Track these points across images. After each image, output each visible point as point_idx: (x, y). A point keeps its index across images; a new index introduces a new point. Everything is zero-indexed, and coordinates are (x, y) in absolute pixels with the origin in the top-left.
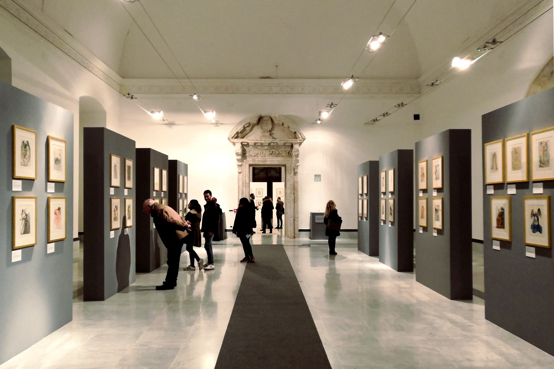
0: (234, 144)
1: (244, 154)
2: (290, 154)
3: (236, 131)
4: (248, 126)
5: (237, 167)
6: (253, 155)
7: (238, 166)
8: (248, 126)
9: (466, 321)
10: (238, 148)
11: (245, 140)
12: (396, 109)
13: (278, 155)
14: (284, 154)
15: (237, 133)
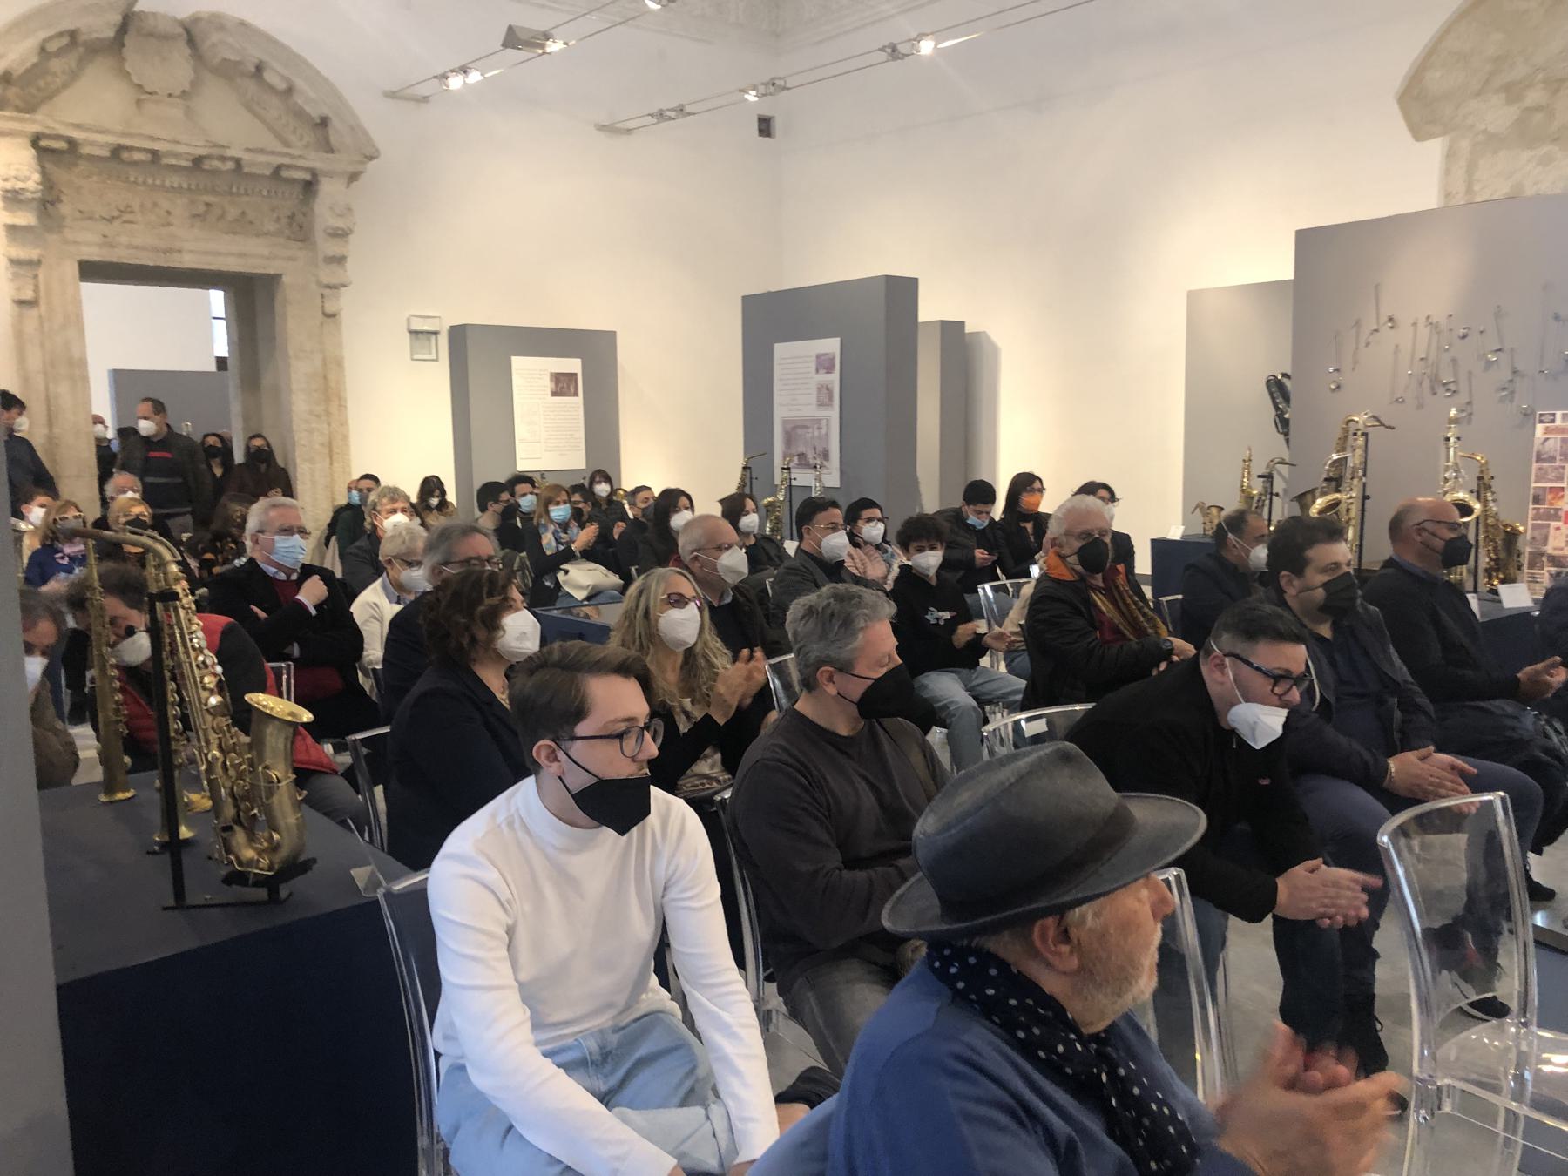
1: (47, 202)
2: (299, 230)
4: (60, 53)
7: (15, 262)
8: (60, 53)
11: (38, 122)
12: (651, 120)
13: (241, 226)
14: (271, 226)
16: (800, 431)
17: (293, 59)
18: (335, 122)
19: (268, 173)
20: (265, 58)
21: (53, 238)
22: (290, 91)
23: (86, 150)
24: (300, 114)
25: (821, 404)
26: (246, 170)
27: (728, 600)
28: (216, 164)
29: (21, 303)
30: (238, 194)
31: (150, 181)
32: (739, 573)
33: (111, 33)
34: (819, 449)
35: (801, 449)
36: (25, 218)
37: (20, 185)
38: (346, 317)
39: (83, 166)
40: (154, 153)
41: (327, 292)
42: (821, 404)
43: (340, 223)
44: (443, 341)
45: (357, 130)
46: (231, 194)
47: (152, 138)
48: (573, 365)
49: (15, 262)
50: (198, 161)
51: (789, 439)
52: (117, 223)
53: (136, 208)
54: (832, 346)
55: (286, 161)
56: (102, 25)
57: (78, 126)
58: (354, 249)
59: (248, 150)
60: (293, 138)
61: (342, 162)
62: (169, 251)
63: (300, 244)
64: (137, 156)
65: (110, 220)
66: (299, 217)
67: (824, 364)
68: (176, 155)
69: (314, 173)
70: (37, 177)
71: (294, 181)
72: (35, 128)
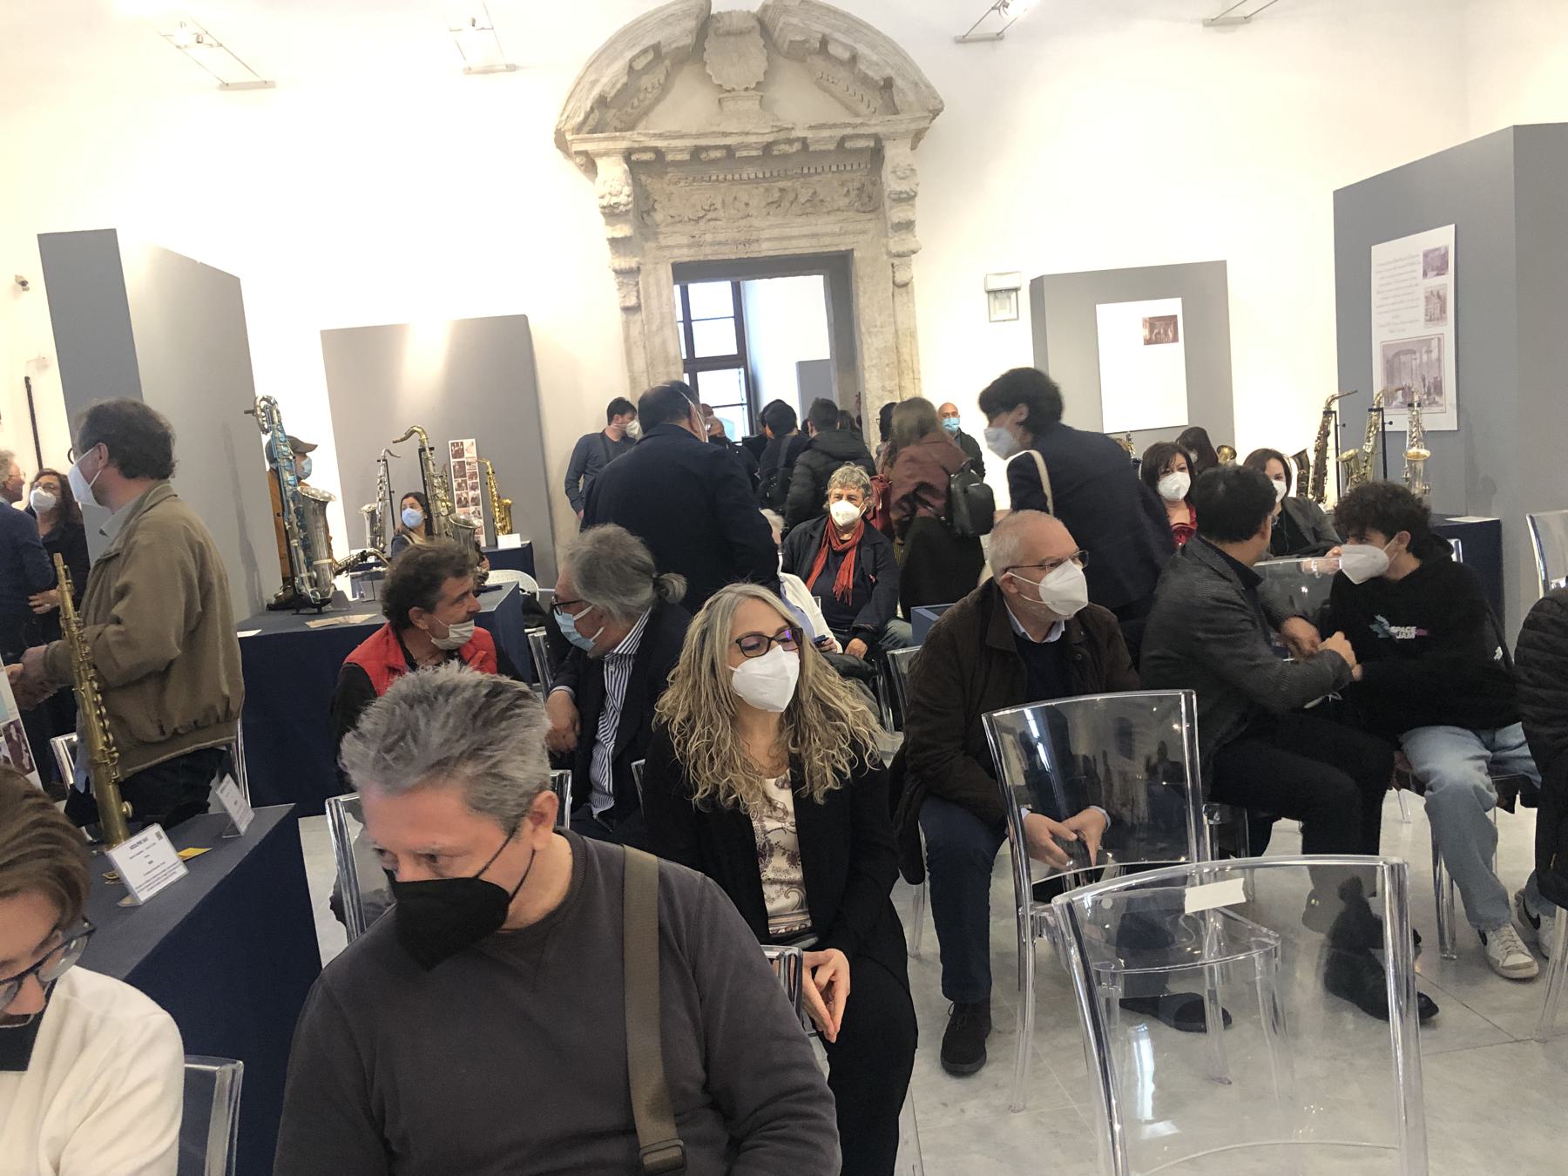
0: (589, 164)
2: (870, 200)
3: (596, 92)
4: (648, 68)
5: (612, 281)
6: (689, 213)
7: (619, 272)
8: (648, 68)
9: (961, 602)
10: (613, 177)
11: (639, 137)
13: (815, 205)
15: (602, 102)
16: (1403, 358)
17: (856, 26)
18: (899, 82)
19: (832, 147)
20: (827, 31)
21: (650, 245)
22: (854, 59)
23: (670, 157)
24: (865, 80)
25: (1430, 319)
26: (811, 148)
27: (1055, 637)
28: (786, 148)
29: (626, 309)
30: (809, 174)
31: (729, 177)
32: (1077, 603)
33: (688, 41)
34: (1430, 380)
35: (1406, 382)
36: (623, 230)
37: (614, 200)
38: (917, 285)
39: (672, 174)
40: (728, 148)
41: (896, 261)
42: (1430, 319)
43: (903, 187)
44: (1025, 295)
45: (920, 84)
46: (803, 175)
47: (725, 134)
48: (1171, 306)
49: (619, 272)
50: (768, 147)
51: (1391, 370)
52: (702, 223)
53: (719, 205)
54: (1443, 237)
55: (849, 131)
56: (680, 34)
57: (660, 136)
58: (919, 213)
59: (811, 128)
60: (862, 108)
61: (904, 123)
62: (748, 242)
63: (870, 216)
64: (714, 154)
65: (698, 220)
66: (869, 188)
67: (1433, 262)
68: (746, 146)
69: (878, 139)
70: (627, 190)
71: (861, 151)
72: (624, 144)
